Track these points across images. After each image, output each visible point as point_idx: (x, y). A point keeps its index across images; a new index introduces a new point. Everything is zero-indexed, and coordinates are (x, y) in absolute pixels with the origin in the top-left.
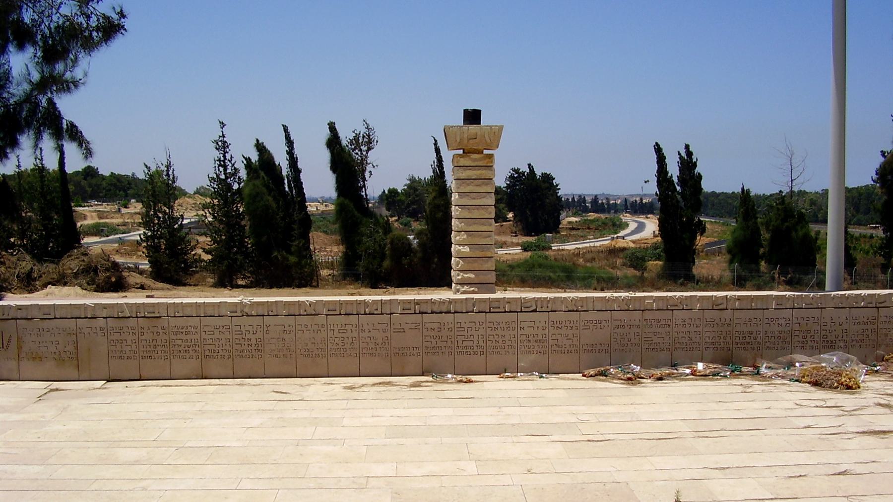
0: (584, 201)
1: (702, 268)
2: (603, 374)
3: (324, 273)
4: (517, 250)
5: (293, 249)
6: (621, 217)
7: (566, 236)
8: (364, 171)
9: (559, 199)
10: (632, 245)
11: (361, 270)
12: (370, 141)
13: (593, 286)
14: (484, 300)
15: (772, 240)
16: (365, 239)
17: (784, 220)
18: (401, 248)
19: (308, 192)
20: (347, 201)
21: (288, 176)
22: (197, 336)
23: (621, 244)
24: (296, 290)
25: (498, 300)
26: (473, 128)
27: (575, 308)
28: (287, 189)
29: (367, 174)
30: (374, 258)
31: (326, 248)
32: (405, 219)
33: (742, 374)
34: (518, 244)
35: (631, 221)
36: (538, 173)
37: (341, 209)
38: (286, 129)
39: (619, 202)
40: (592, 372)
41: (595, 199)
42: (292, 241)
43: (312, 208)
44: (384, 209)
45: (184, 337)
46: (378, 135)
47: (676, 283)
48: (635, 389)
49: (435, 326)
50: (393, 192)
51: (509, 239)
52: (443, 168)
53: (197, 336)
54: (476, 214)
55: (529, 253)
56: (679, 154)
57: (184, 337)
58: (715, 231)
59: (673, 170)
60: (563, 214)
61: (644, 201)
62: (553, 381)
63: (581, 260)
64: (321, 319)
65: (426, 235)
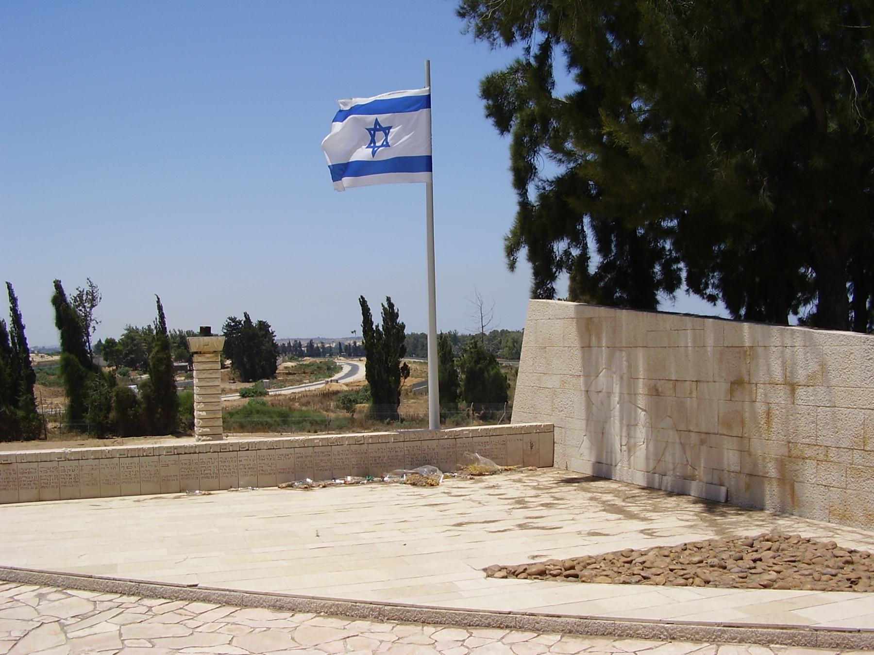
0: (300, 345)
1: (411, 407)
2: (291, 486)
3: (50, 425)
4: (236, 397)
5: (20, 404)
6: (336, 361)
7: (282, 381)
8: (88, 327)
9: (275, 345)
10: (345, 388)
11: (88, 421)
12: (93, 299)
13: (307, 429)
14: (217, 445)
15: (469, 380)
16: (91, 392)
17: (477, 362)
18: (127, 400)
19: (30, 344)
20: (72, 356)
21: (12, 332)
22: (36, 475)
23: (335, 387)
24: (25, 443)
25: (225, 444)
26: (207, 339)
27: (272, 447)
28: (10, 343)
29: (91, 330)
30: (101, 410)
31: (52, 402)
32: (123, 369)
33: (373, 482)
34: (236, 391)
35: (345, 364)
36: (254, 321)
37: (66, 365)
38: (9, 287)
39: (334, 345)
40: (284, 485)
41: (311, 344)
42: (19, 396)
43: (35, 358)
44: (102, 359)
45: (27, 475)
46: (101, 292)
47: (383, 423)
48: (309, 493)
49: (187, 462)
50: (110, 342)
51: (227, 386)
52: (165, 324)
53: (36, 475)
54: (209, 391)
55: (247, 400)
56: (383, 306)
57: (27, 475)
58: (424, 372)
59: (378, 320)
60: (280, 360)
61: (358, 344)
62: (260, 491)
63: (297, 404)
64: (116, 461)
65: (150, 387)
